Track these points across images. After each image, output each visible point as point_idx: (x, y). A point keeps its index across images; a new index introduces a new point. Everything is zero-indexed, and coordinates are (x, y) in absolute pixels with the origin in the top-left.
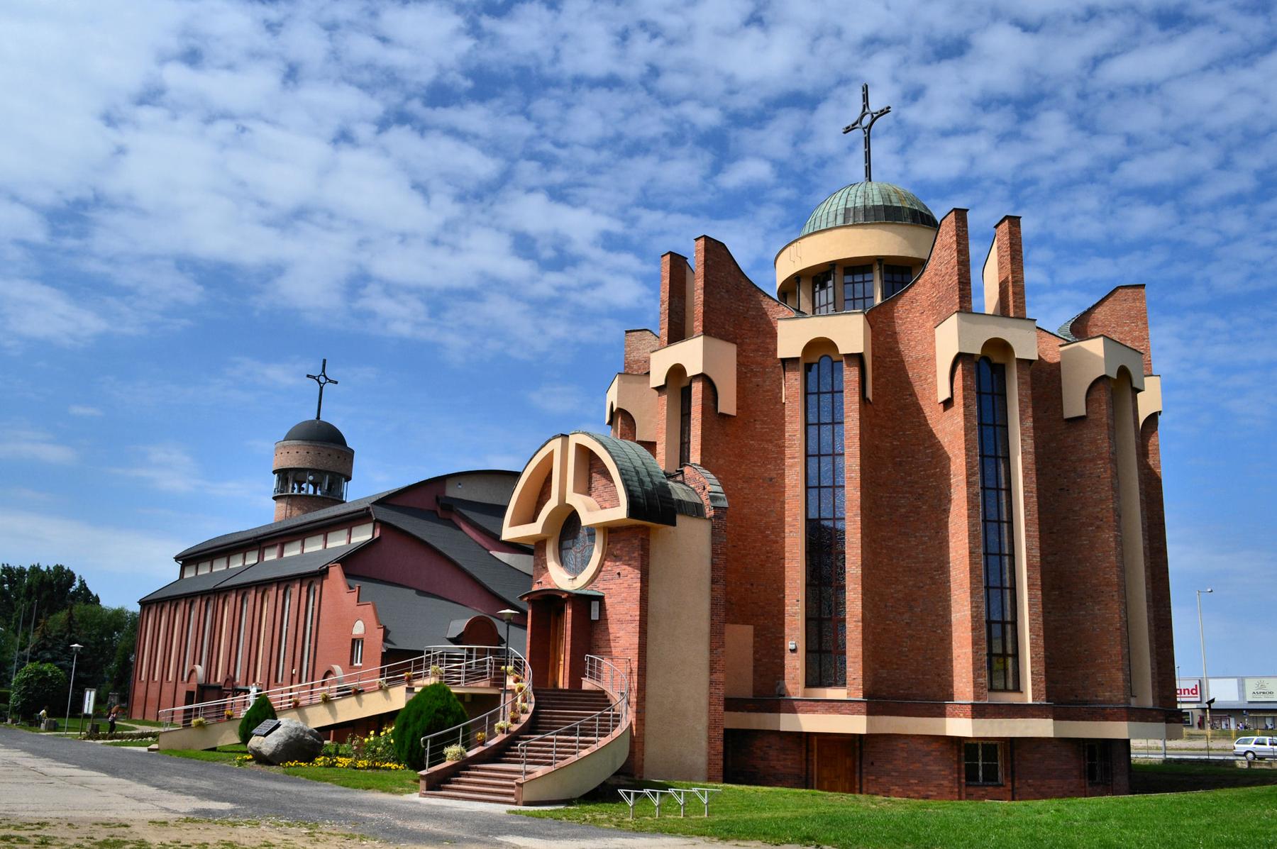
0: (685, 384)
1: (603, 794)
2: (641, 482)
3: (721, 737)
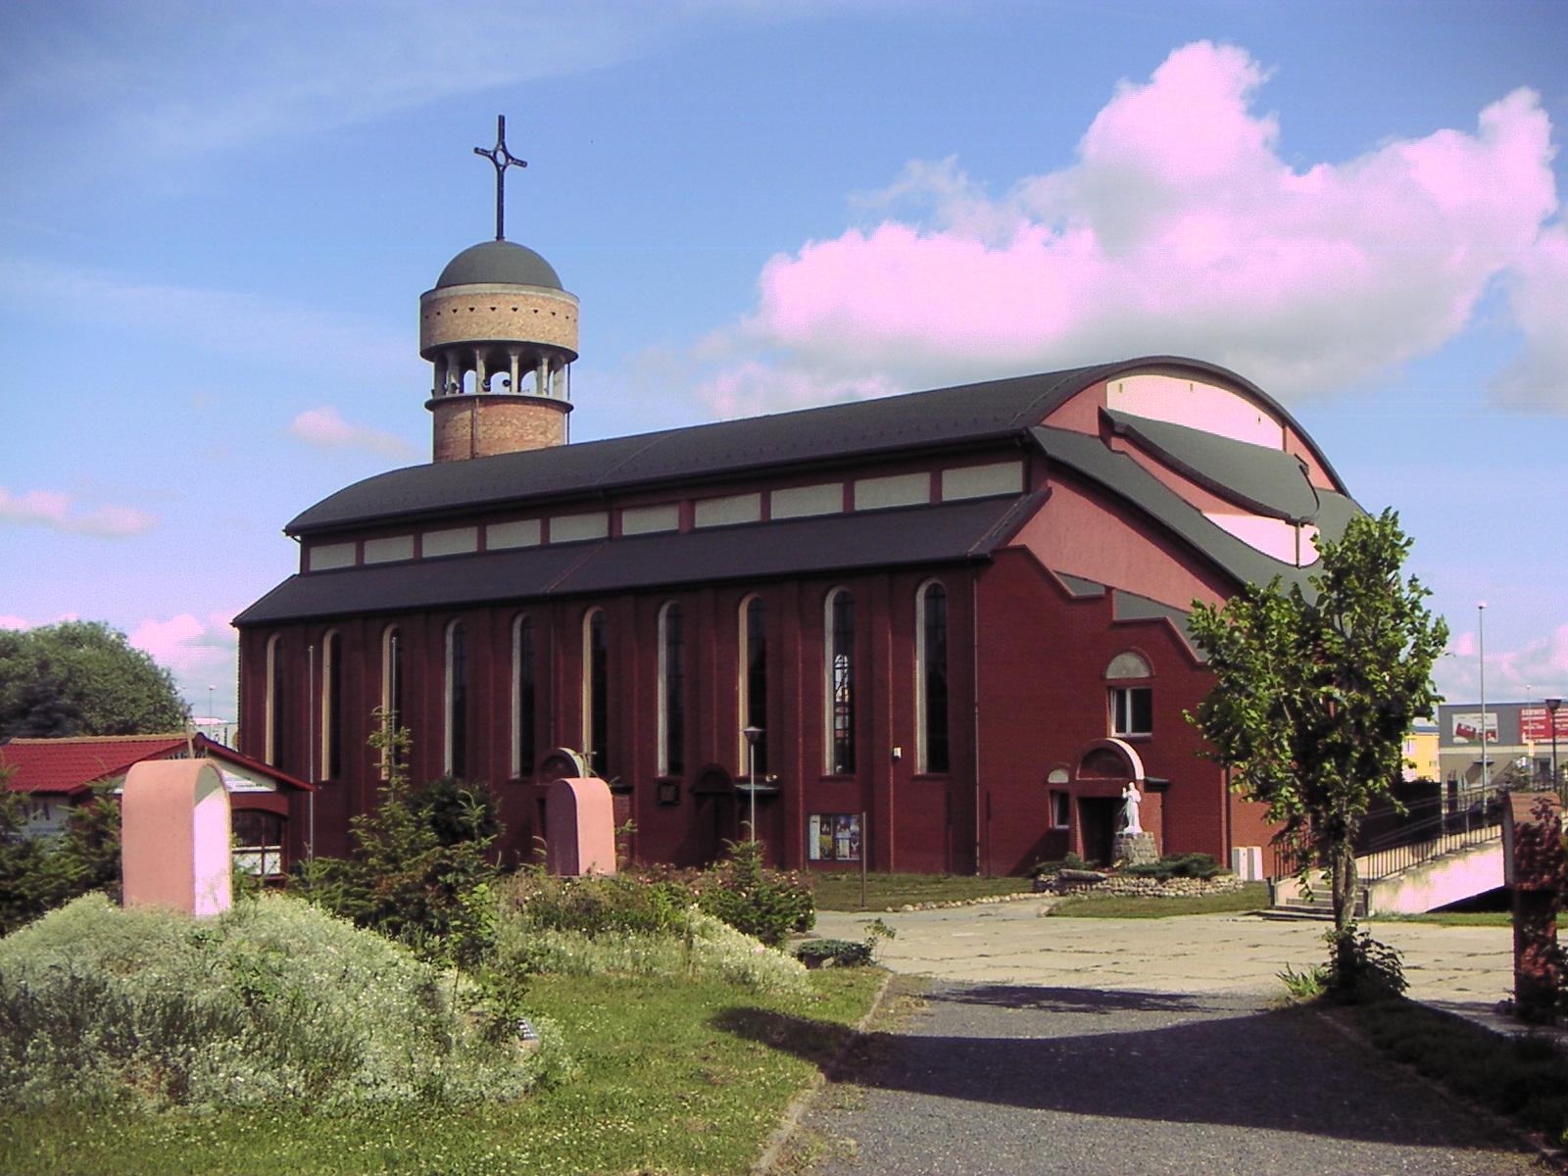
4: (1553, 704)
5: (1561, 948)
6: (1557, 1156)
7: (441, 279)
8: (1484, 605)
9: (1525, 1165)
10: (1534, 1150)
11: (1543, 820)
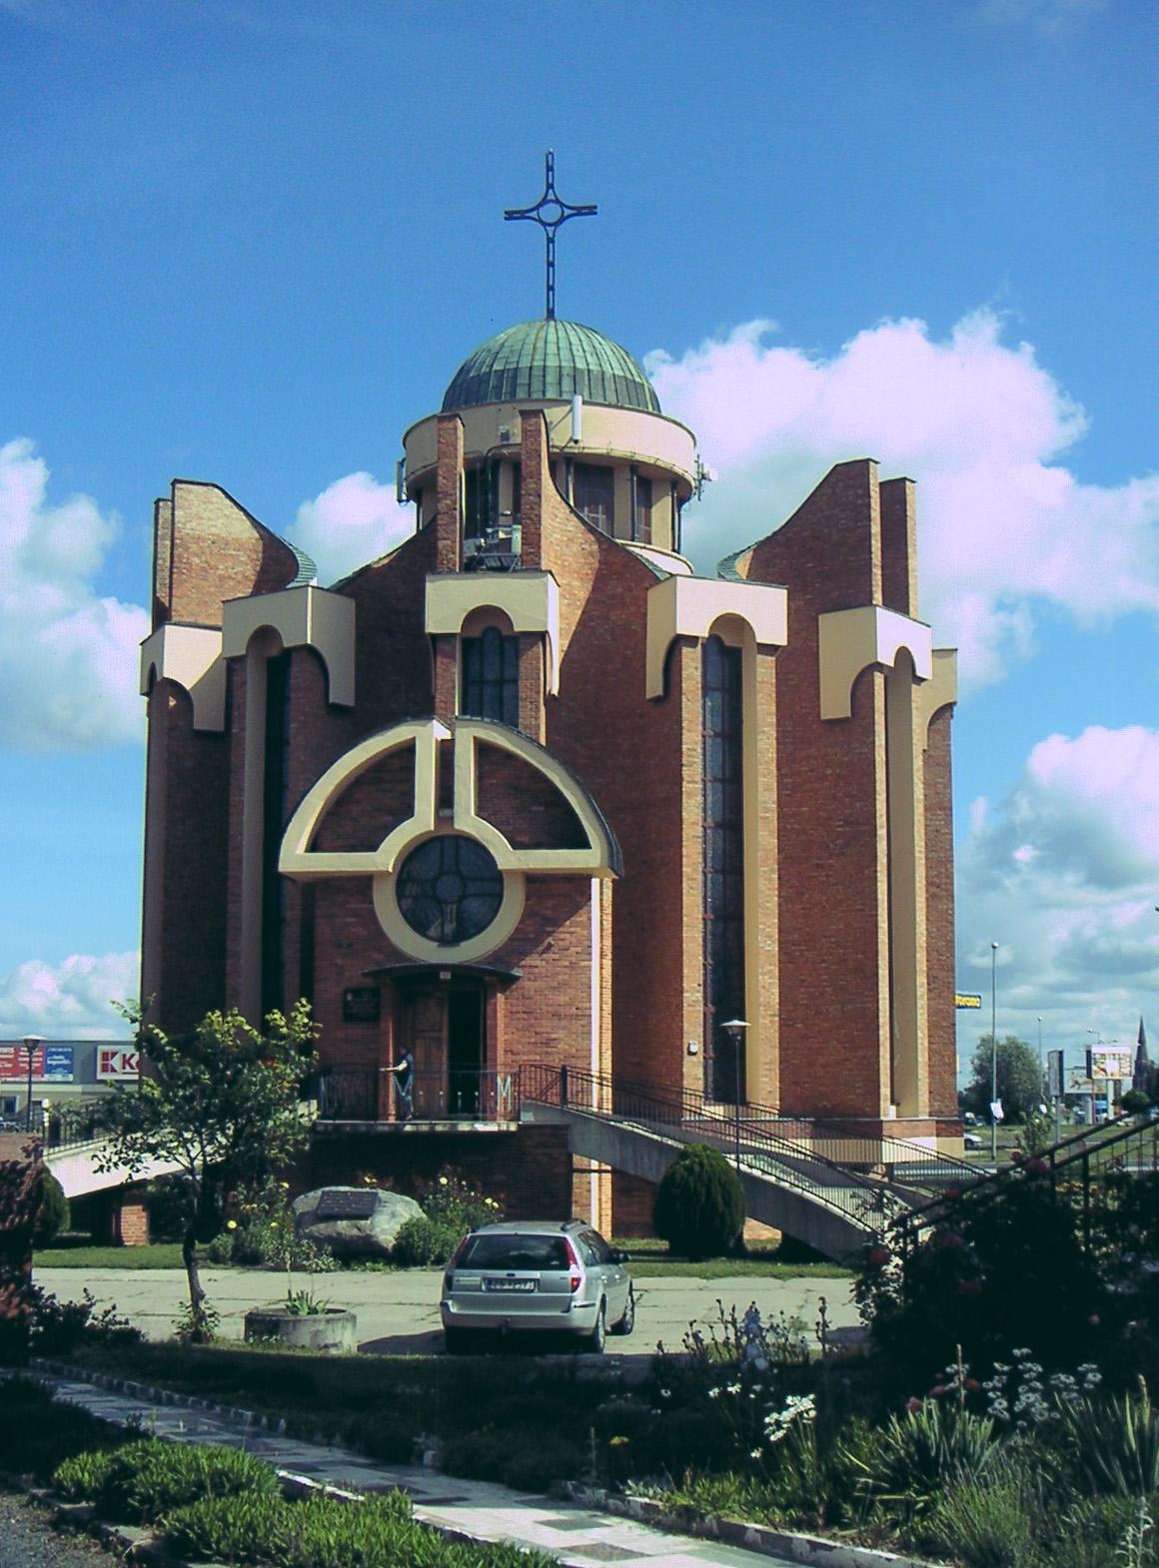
4: (30, 1045)
5: (36, 1288)
6: (46, 1496)
8: (996, 944)
9: (15, 1507)
10: (22, 1491)
11: (32, 1159)
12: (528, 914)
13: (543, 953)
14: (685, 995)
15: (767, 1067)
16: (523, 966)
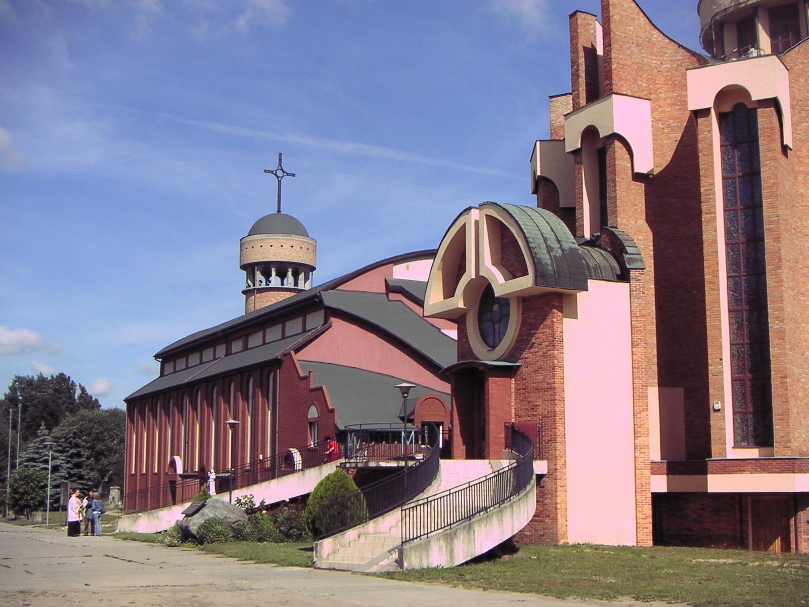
0: (600, 145)
1: (124, 539)
2: (549, 249)
3: (650, 500)
7: (250, 231)
12: (524, 323)
13: (531, 348)
14: (710, 368)
15: (780, 417)
16: (522, 358)
